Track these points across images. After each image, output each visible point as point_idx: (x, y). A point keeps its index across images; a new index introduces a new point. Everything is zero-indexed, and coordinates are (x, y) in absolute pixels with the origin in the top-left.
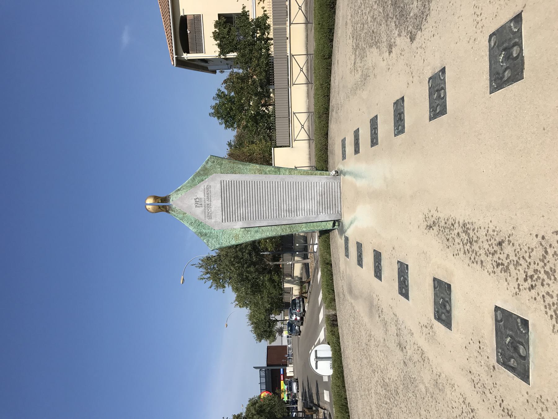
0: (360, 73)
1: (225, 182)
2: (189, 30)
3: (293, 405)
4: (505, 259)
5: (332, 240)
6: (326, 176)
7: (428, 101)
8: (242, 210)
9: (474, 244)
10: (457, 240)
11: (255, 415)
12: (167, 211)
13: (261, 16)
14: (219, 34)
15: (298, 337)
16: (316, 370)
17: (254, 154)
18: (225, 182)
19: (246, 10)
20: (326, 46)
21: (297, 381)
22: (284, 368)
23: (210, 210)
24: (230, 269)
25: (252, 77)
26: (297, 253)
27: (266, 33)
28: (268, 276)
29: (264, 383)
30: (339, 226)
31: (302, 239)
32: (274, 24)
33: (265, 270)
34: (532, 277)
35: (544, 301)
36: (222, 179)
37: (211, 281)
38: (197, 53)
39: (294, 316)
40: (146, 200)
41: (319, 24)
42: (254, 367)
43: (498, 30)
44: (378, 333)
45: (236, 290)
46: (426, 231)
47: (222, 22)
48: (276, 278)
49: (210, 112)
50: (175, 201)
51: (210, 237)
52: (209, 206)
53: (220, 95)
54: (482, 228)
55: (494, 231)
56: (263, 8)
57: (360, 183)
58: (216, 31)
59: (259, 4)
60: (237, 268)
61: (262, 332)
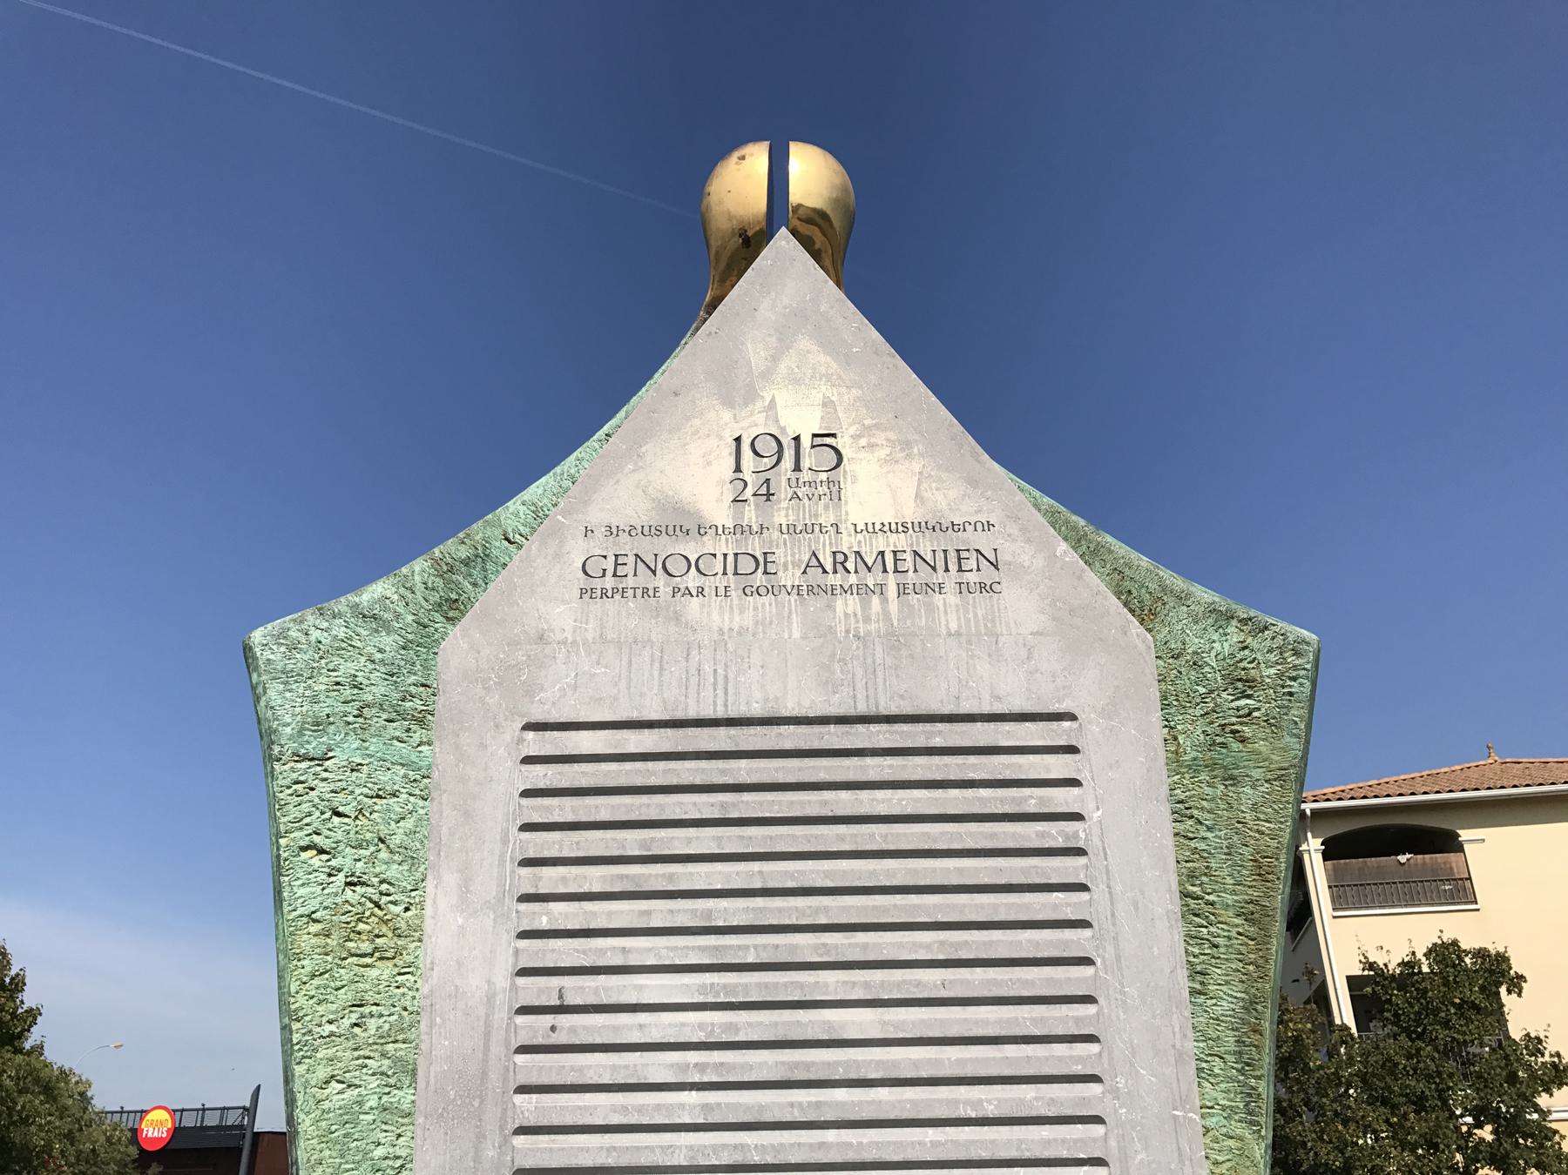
1: (1056, 766)
2: (1411, 861)
18: (1056, 766)
23: (692, 580)
29: (202, 1121)
36: (1090, 732)
38: (1330, 887)
42: (259, 1086)
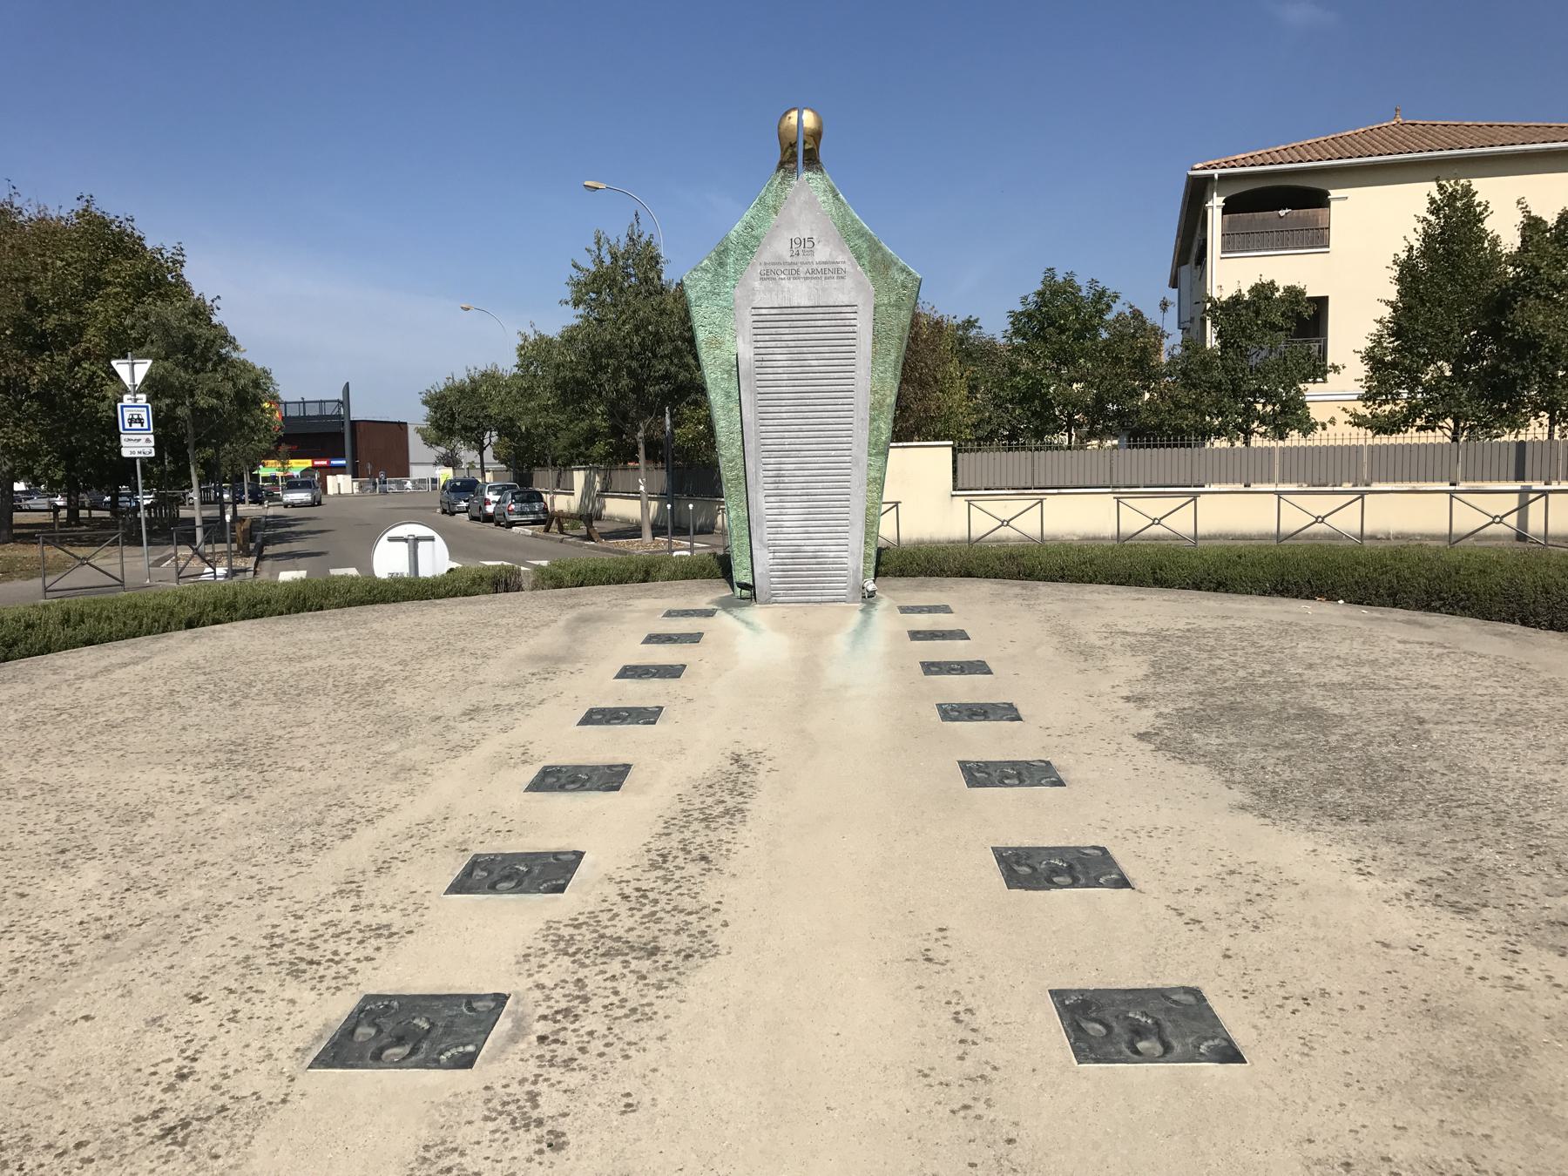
0: (1099, 643)
1: (852, 316)
3: (249, 492)
4: (675, 864)
5: (707, 583)
6: (862, 567)
7: (1003, 759)
8: (781, 359)
9: (703, 825)
10: (709, 801)
11: (234, 385)
12: (782, 165)
13: (1312, 415)
14: (1267, 298)
15: (437, 508)
16: (385, 538)
17: (941, 391)
18: (852, 316)
19: (1330, 376)
20: (1185, 573)
21: (316, 503)
22: (349, 468)
23: (783, 276)
24: (624, 322)
25: (1147, 388)
26: (669, 506)
27: (1262, 430)
28: (605, 427)
30: (741, 598)
31: (706, 519)
32: (1283, 450)
33: (620, 422)
34: (645, 897)
35: (602, 911)
37: (593, 269)
38: (1223, 235)
39: (497, 498)
40: (812, 111)
41: (1240, 557)
43: (1111, 858)
44: (494, 672)
45: (569, 339)
46: (728, 753)
47: (1300, 309)
48: (600, 448)
49: (1057, 271)
50: (810, 186)
51: (716, 274)
52: (794, 274)
53: (1102, 299)
54: (734, 835)
55: (728, 850)
56: (1332, 421)
57: (840, 642)
58: (1278, 290)
59: (1344, 409)
60: (628, 341)
61: (451, 409)
